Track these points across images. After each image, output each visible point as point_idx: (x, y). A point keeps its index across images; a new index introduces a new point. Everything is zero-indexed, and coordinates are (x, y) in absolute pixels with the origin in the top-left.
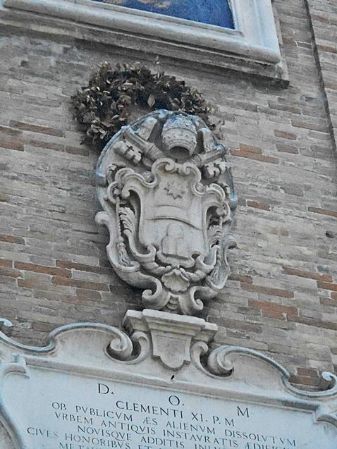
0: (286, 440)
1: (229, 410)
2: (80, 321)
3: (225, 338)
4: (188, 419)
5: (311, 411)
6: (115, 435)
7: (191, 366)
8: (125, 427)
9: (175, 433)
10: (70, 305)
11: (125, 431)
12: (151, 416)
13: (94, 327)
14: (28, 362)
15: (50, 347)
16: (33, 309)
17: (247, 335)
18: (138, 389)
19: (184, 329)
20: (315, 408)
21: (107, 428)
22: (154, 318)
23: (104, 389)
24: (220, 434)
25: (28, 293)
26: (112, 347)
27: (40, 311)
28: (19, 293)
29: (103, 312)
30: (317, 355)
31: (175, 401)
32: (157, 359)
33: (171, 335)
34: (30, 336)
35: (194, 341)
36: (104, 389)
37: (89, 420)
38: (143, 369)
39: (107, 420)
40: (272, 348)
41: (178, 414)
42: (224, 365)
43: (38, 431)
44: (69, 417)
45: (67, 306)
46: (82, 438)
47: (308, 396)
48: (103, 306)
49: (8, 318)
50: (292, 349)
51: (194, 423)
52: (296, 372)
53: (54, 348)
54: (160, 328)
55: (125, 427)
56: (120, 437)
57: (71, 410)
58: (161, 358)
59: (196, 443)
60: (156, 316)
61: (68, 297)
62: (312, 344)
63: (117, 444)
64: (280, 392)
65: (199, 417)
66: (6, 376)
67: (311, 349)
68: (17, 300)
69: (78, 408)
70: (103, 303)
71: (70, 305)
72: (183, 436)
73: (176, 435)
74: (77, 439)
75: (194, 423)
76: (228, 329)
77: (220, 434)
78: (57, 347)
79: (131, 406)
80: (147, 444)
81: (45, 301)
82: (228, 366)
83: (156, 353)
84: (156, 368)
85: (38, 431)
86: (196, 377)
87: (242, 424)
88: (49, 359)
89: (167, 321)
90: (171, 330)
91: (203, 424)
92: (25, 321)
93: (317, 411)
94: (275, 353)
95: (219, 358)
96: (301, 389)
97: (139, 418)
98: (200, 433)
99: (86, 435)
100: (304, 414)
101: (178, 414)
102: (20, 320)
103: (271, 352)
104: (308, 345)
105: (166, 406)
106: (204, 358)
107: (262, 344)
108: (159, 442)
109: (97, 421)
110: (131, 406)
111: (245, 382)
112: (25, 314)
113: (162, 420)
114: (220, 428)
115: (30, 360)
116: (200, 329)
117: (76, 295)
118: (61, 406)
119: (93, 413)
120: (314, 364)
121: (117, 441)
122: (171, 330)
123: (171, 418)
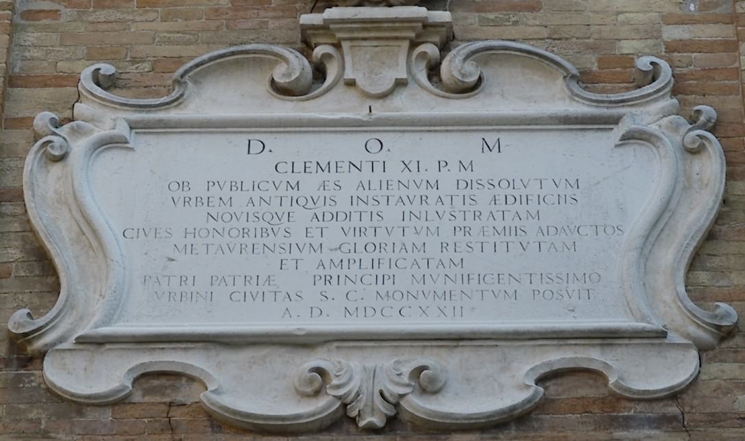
0: (563, 181)
1: (466, 146)
2: (231, 45)
3: (475, 30)
4: (395, 172)
5: (611, 126)
6: (268, 217)
7: (412, 85)
8: (286, 202)
9: (370, 199)
10: (217, 23)
11: (286, 206)
12: (332, 177)
13: (247, 52)
14: (133, 126)
15: (174, 95)
16: (157, 39)
17: (515, 19)
18: (196, 136)
19: (395, 29)
20: (616, 120)
21: (257, 208)
22: (343, 21)
23: (256, 147)
24: (447, 187)
25: (152, 15)
26: (280, 80)
27: (169, 42)
28: (137, 19)
29: (272, 24)
30: (637, 30)
31: (374, 146)
32: (351, 84)
33: (375, 43)
34: (148, 83)
35: (414, 45)
36: (256, 147)
37: (433, 231)
38: (328, 105)
39: (256, 195)
40: (555, 32)
41: (378, 167)
42: (463, 75)
43: (141, 231)
44: (193, 200)
45: (213, 25)
46: (211, 231)
47: (611, 102)
48: (270, 14)
49: (107, 61)
50: (593, 29)
51: (405, 177)
52: (596, 64)
53: (182, 95)
54: (356, 35)
55: (286, 202)
56: (276, 220)
57: (198, 190)
58: (357, 81)
59: (404, 208)
60: (345, 17)
61: (217, 10)
62: (627, 14)
63: (270, 231)
64: (555, 99)
65: (413, 167)
66: (94, 155)
67: (628, 23)
68: (133, 30)
69: (211, 184)
70: (274, 10)
71: (217, 23)
72: (383, 201)
73: (371, 202)
74: (204, 233)
75: (405, 177)
76: (483, 15)
77: (447, 187)
78: (187, 94)
79: (299, 167)
80: (321, 224)
81: (180, 24)
82: (470, 75)
83: (349, 74)
84: (351, 96)
85: (141, 231)
86: (420, 102)
87: (489, 166)
88: (173, 114)
89: (363, 21)
90: (372, 34)
91: (423, 176)
92: (142, 61)
93: (620, 124)
94: (560, 39)
95: (452, 67)
96: (603, 91)
97: (310, 184)
98: (413, 191)
99: (219, 225)
100: (599, 134)
101: (378, 167)
102: (134, 61)
103: (554, 39)
104: (621, 17)
105: (359, 156)
106: (434, 71)
107: (537, 29)
108: (341, 216)
109: (240, 198)
110: (299, 167)
111: (502, 96)
112: (142, 50)
113: (349, 180)
114: (448, 180)
115: (137, 122)
116: (420, 25)
117: (230, 5)
118: (182, 185)
119: (234, 188)
120: (627, 47)
121: (269, 227)
122: (372, 34)
123: (366, 174)
